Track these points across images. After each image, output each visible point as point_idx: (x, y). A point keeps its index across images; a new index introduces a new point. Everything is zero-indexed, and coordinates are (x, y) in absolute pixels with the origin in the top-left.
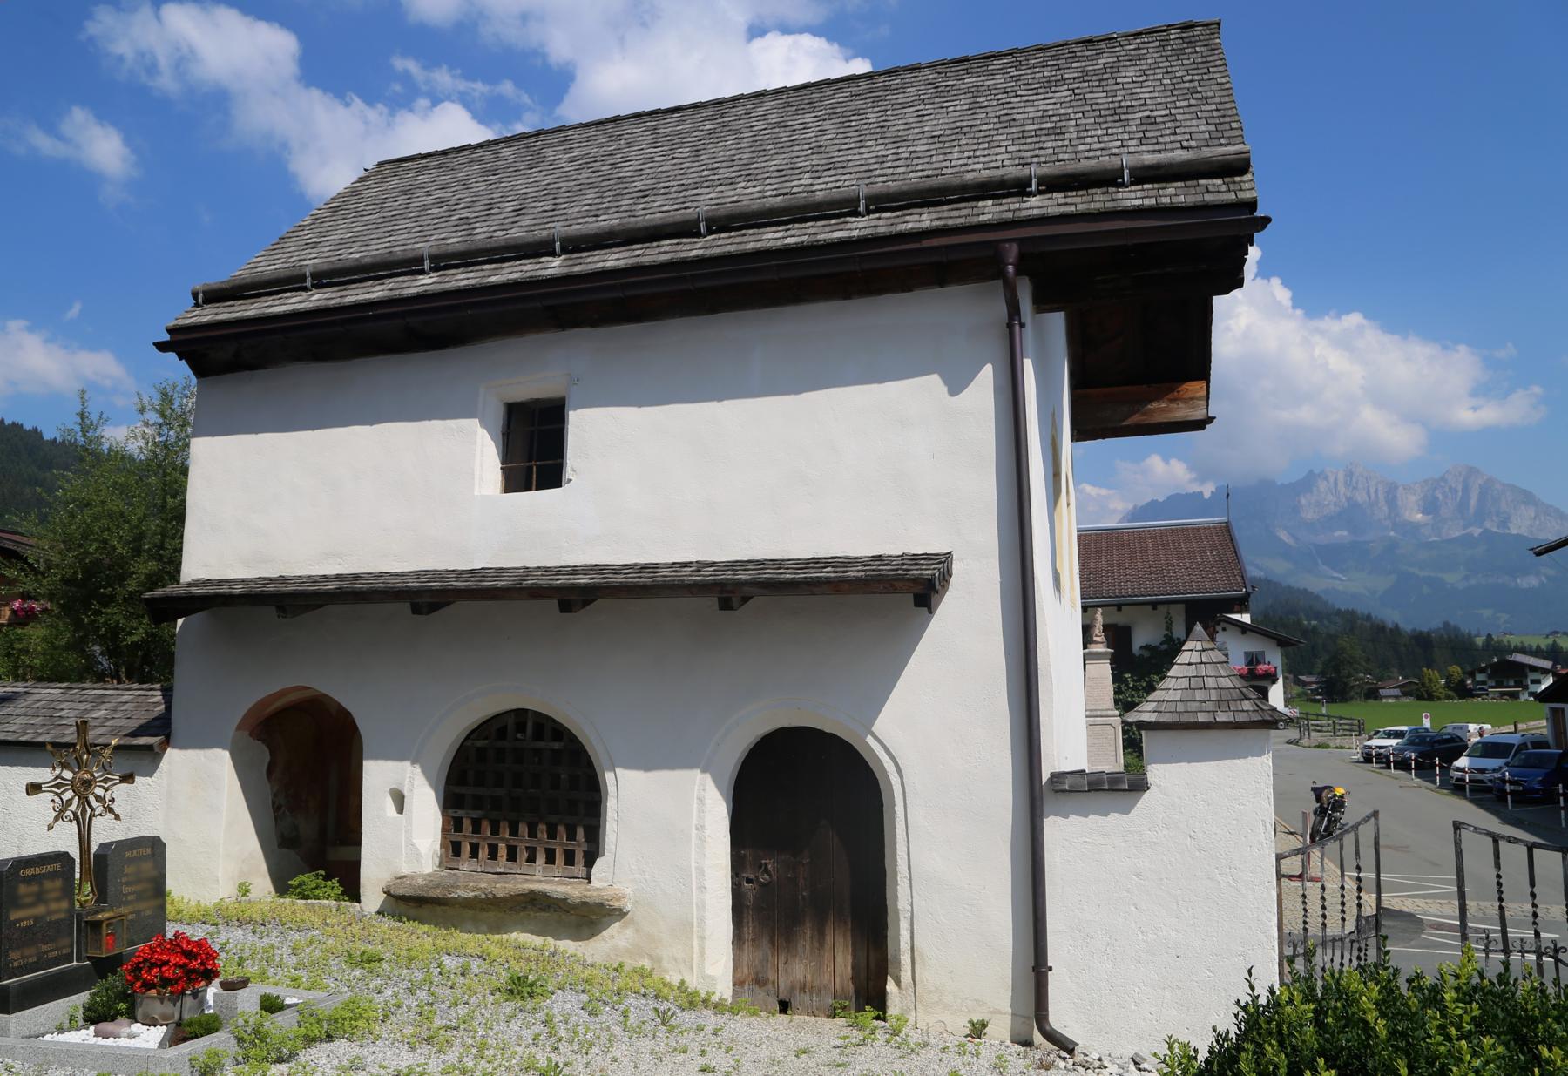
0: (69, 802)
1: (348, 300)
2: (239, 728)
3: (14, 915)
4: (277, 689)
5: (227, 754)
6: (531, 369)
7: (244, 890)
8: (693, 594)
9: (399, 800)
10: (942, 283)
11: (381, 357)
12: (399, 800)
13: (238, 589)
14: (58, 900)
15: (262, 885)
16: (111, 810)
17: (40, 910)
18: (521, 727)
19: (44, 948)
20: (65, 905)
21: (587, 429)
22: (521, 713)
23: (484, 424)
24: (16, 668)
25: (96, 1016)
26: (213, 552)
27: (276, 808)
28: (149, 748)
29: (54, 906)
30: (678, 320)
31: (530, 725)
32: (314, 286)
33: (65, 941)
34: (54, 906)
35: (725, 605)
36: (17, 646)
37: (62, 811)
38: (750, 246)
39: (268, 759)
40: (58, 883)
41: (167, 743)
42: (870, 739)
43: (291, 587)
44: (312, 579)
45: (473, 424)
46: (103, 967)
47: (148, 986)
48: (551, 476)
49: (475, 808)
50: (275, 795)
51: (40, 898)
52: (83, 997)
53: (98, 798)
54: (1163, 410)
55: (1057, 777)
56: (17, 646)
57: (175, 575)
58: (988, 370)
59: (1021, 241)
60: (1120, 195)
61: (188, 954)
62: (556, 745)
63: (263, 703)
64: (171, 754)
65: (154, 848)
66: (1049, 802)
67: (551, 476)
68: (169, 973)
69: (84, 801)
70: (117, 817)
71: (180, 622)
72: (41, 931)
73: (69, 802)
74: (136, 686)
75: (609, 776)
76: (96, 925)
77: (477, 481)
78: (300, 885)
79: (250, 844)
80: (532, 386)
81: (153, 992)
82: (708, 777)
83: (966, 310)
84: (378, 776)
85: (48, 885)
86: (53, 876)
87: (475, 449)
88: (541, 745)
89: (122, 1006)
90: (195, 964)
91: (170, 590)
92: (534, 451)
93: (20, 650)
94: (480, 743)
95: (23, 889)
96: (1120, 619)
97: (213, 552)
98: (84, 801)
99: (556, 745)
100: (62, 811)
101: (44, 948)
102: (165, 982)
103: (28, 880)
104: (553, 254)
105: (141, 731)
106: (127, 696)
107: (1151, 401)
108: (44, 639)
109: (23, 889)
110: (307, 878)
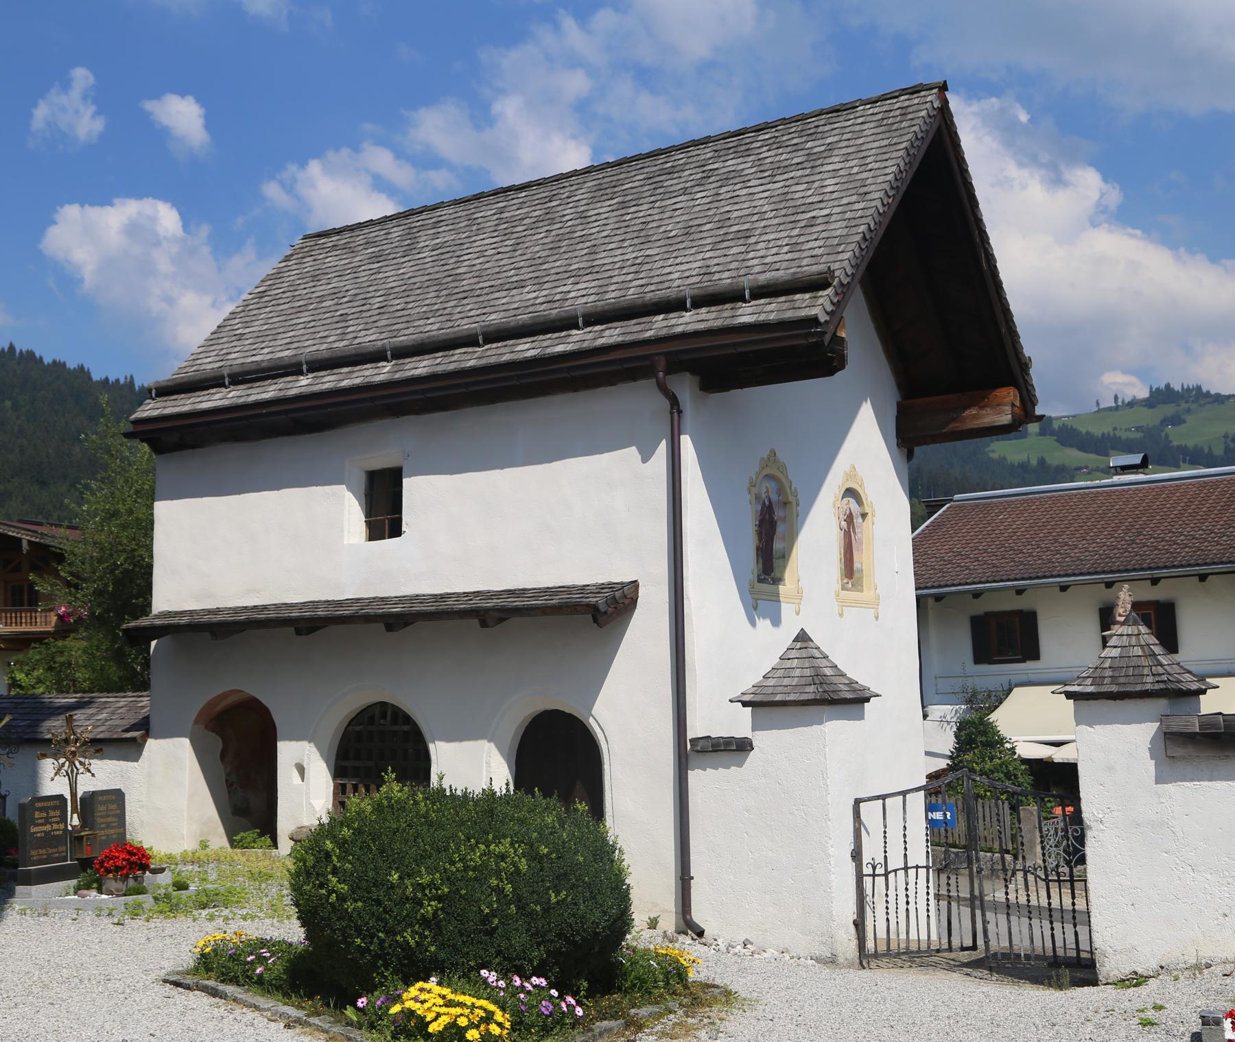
0: (63, 765)
1: (252, 398)
2: (196, 722)
3: (33, 830)
4: (219, 692)
5: (186, 742)
6: (381, 446)
7: (204, 845)
8: (461, 618)
9: (301, 770)
10: (635, 379)
11: (280, 439)
12: (301, 770)
13: (185, 620)
14: (58, 823)
15: (219, 840)
16: (89, 771)
17: (48, 828)
18: (384, 715)
19: (51, 851)
20: (62, 826)
21: (413, 488)
22: (383, 704)
23: (350, 489)
24: (59, 682)
25: (77, 890)
26: (173, 592)
27: (230, 785)
28: (133, 740)
29: (55, 826)
30: (475, 408)
31: (389, 713)
32: (230, 383)
33: (61, 848)
34: (55, 826)
35: (484, 624)
36: (59, 659)
37: (59, 770)
38: (505, 358)
39: (220, 746)
40: (58, 813)
41: (147, 735)
42: (591, 720)
43: (219, 618)
44: (236, 610)
45: (342, 489)
46: (85, 864)
47: (108, 871)
48: (395, 530)
49: (354, 776)
50: (228, 775)
51: (47, 821)
52: (74, 882)
53: (81, 763)
54: (974, 417)
55: (695, 741)
56: (59, 659)
57: (146, 607)
58: (664, 442)
59: (666, 354)
60: (740, 312)
61: (130, 853)
62: (406, 728)
63: (211, 704)
64: (151, 743)
65: (117, 797)
66: (693, 758)
67: (395, 530)
68: (119, 863)
69: (72, 764)
70: (93, 775)
71: (153, 643)
72: (50, 840)
73: (63, 765)
74: (130, 694)
75: (431, 747)
76: (80, 839)
77: (346, 533)
78: (241, 840)
79: (208, 810)
80: (382, 460)
81: (111, 875)
82: (492, 745)
83: (640, 399)
84: (289, 752)
85: (52, 813)
86: (55, 808)
87: (345, 508)
88: (396, 728)
89: (95, 885)
90: (134, 858)
91: (144, 622)
92: (385, 518)
93: (62, 664)
94: (357, 728)
95: (37, 815)
96: (1149, 594)
97: (173, 592)
98: (72, 764)
99: (406, 728)
100: (59, 770)
101: (51, 851)
102: (118, 869)
103: (41, 810)
104: (386, 360)
105: (133, 728)
106: (123, 702)
107: (968, 407)
108: (85, 651)
109: (37, 815)
110: (249, 835)
